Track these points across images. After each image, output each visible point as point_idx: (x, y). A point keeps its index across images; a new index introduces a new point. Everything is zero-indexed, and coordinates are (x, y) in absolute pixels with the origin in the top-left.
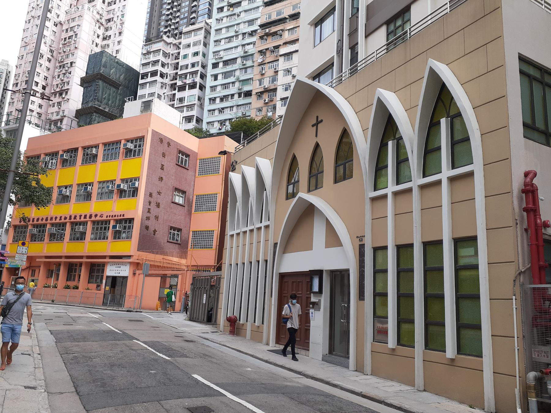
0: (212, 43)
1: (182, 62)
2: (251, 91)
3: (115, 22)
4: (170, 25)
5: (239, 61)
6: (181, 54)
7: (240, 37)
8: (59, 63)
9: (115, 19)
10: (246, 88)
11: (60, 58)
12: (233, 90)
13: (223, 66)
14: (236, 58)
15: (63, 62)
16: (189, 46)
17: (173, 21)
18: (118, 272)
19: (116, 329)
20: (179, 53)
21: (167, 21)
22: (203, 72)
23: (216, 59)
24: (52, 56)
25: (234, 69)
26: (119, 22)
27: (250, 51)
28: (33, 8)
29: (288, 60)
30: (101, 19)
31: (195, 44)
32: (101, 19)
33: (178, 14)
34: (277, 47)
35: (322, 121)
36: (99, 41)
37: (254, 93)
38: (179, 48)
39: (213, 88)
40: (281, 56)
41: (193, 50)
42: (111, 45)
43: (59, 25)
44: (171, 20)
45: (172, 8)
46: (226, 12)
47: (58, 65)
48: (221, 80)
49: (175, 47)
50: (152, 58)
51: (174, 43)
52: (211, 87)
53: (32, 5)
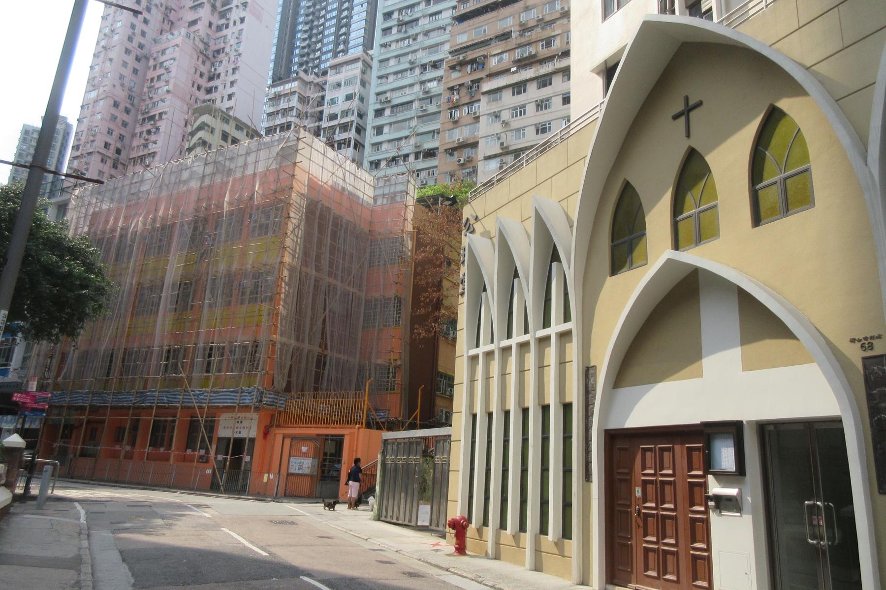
0: (374, 81)
1: (327, 110)
2: (437, 148)
3: (227, 54)
4: (307, 63)
5: (416, 105)
6: (327, 98)
7: (417, 71)
8: (143, 114)
9: (227, 50)
10: (428, 145)
11: (144, 108)
12: (407, 147)
13: (392, 112)
14: (411, 102)
15: (147, 113)
16: (339, 85)
17: (311, 56)
18: (238, 430)
19: (252, 542)
20: (323, 97)
21: (302, 56)
22: (361, 122)
23: (381, 103)
24: (132, 105)
25: (409, 116)
26: (233, 54)
27: (433, 90)
28: (105, 35)
29: (495, 100)
30: (206, 50)
31: (348, 83)
32: (206, 50)
33: (319, 46)
34: (478, 81)
35: (699, 104)
36: (203, 82)
37: (441, 150)
38: (323, 89)
39: (377, 145)
40: (483, 94)
41: (341, 94)
42: (221, 88)
43: (143, 60)
44: (308, 54)
45: (310, 37)
46: (395, 34)
47: (140, 117)
48: (388, 134)
49: (318, 88)
50: (283, 105)
51: (315, 81)
52: (373, 145)
53: (104, 31)
